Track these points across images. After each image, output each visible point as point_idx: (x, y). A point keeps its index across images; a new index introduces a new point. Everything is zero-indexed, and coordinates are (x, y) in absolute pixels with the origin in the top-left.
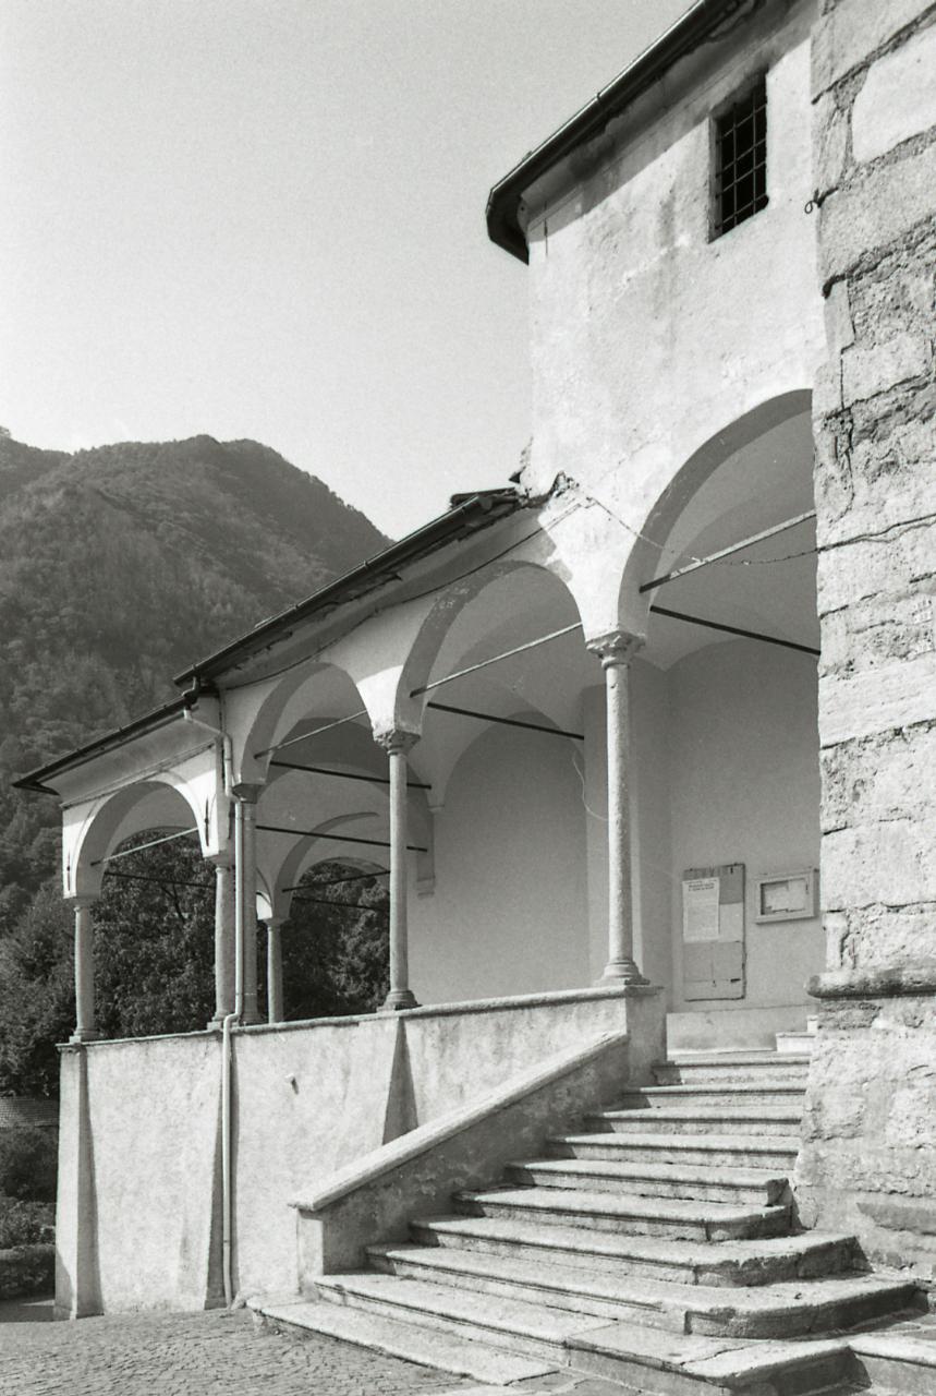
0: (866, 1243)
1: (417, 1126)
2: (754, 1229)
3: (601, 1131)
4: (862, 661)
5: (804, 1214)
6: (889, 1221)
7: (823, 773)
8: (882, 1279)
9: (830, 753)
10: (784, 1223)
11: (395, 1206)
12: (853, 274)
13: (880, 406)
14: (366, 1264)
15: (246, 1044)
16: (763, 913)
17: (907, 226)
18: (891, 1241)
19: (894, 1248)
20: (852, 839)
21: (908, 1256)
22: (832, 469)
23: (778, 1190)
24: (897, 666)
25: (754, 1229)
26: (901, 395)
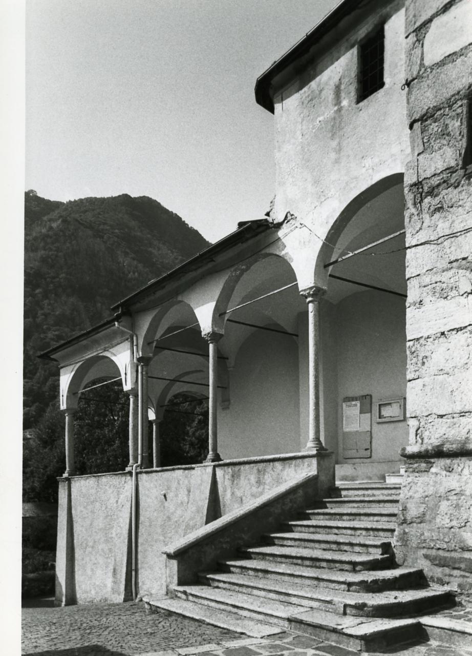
0: (426, 572)
4: (427, 300)
7: (408, 352)
8: (435, 590)
9: (411, 343)
10: (389, 562)
11: (211, 553)
17: (448, 96)
18: (438, 572)
19: (440, 575)
21: (447, 579)
23: (386, 547)
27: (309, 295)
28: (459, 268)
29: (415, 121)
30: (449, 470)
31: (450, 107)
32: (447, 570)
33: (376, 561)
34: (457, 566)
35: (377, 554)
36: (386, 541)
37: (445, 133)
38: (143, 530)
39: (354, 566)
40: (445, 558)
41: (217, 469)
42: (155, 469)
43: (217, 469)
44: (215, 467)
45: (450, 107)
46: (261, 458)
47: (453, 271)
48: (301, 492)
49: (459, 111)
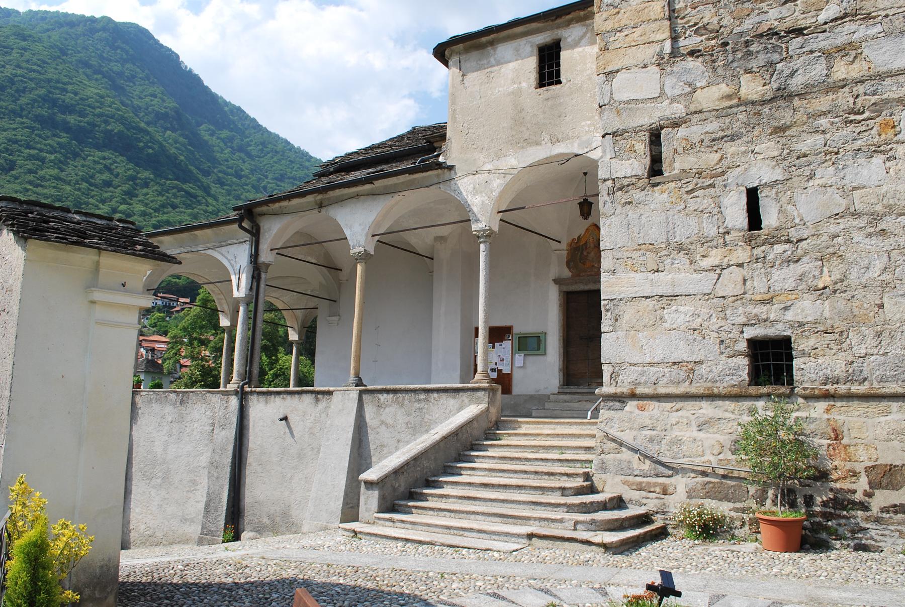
0: (625, 497)
1: (368, 468)
2: (579, 491)
3: (453, 474)
4: (620, 270)
5: (598, 485)
6: (635, 487)
7: (603, 309)
8: (632, 511)
9: (606, 302)
10: (592, 490)
11: (402, 484)
12: (614, 134)
13: (626, 182)
14: (393, 509)
15: (264, 411)
16: (235, 523)
17: (635, 125)
18: (636, 495)
19: (638, 497)
20: (615, 337)
21: (644, 501)
22: (606, 198)
23: (587, 477)
24: (633, 274)
25: (579, 491)
26: (634, 180)
27: (482, 236)
28: (647, 250)
29: (607, 134)
30: (642, 409)
31: (636, 133)
32: (644, 493)
33: (583, 487)
34: (652, 490)
35: (579, 482)
36: (586, 470)
37: (632, 149)
38: (656, 413)
39: (563, 491)
40: (641, 483)
41: (365, 397)
42: (291, 388)
43: (365, 397)
44: (361, 393)
45: (636, 133)
46: (423, 386)
47: (641, 252)
48: (475, 424)
49: (643, 138)
